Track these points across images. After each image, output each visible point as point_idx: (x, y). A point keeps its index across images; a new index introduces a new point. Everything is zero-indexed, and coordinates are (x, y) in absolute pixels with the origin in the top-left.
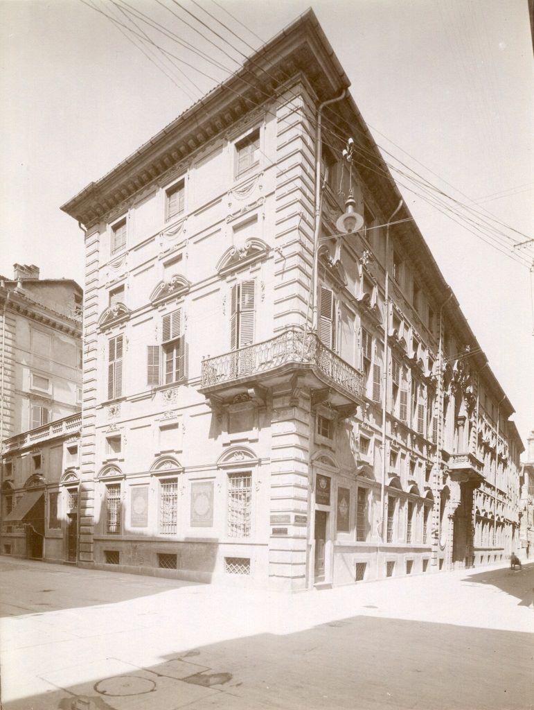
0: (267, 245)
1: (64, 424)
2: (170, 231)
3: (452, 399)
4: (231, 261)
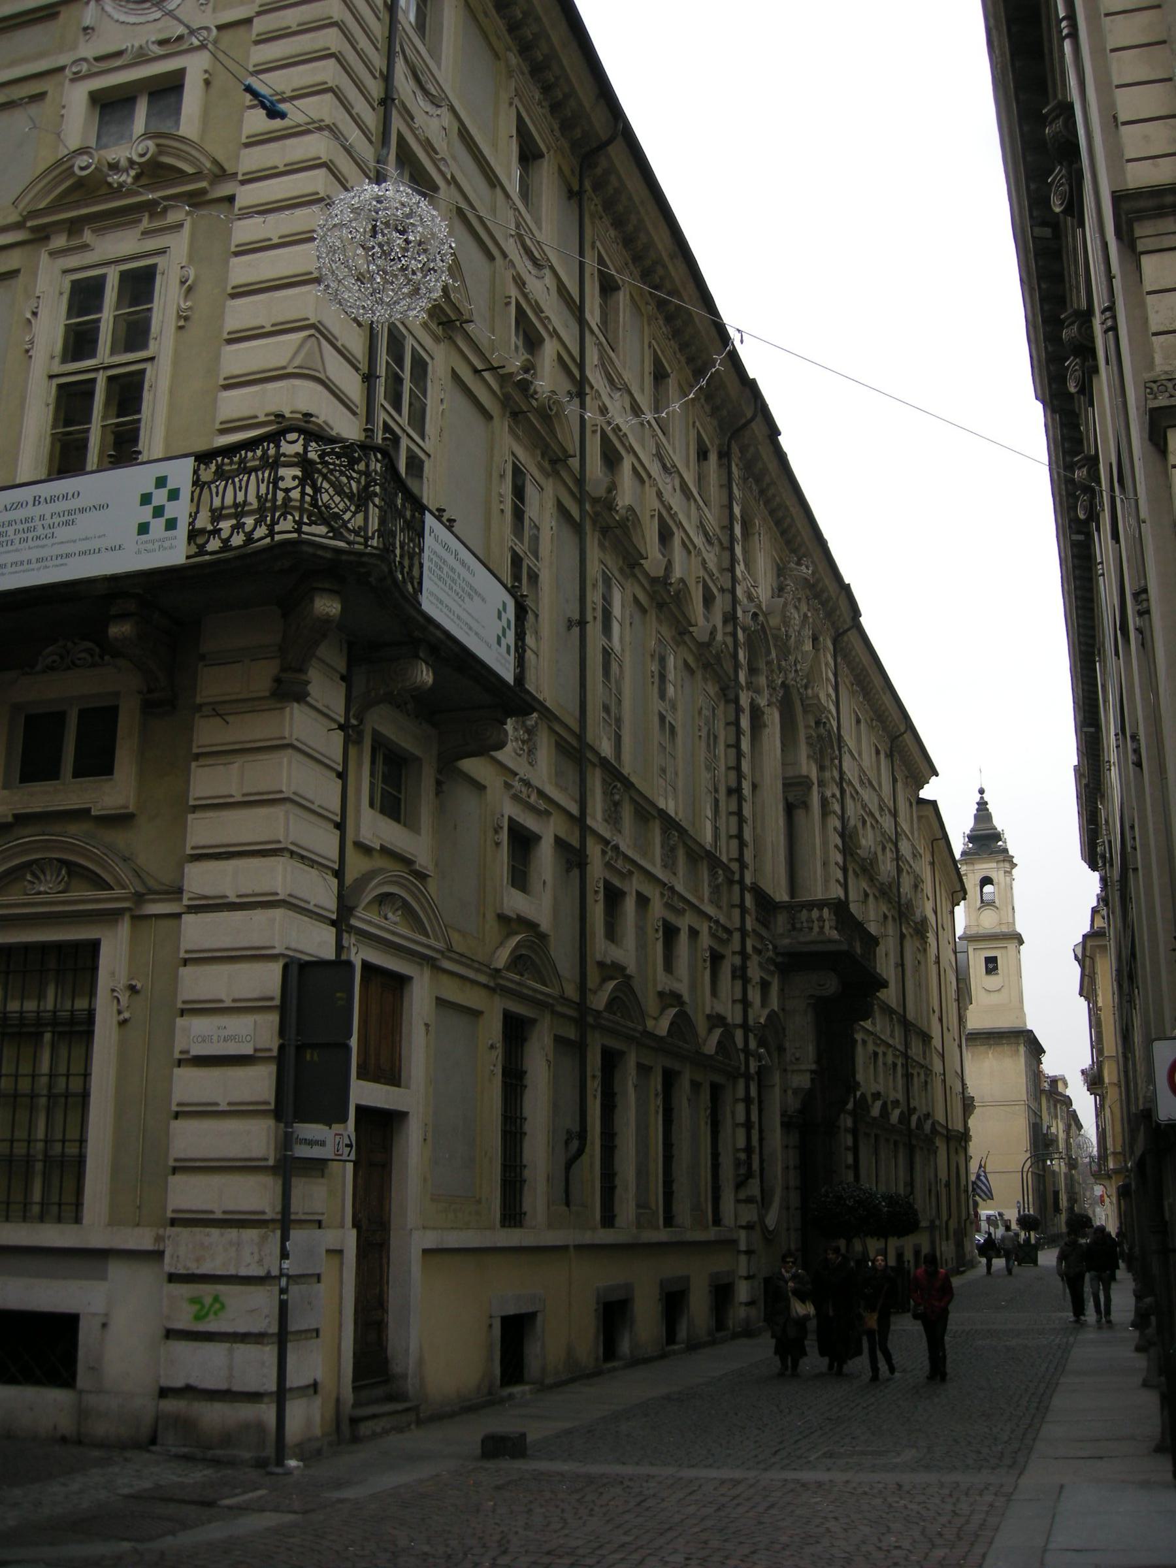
0: (215, 162)
3: (773, 718)
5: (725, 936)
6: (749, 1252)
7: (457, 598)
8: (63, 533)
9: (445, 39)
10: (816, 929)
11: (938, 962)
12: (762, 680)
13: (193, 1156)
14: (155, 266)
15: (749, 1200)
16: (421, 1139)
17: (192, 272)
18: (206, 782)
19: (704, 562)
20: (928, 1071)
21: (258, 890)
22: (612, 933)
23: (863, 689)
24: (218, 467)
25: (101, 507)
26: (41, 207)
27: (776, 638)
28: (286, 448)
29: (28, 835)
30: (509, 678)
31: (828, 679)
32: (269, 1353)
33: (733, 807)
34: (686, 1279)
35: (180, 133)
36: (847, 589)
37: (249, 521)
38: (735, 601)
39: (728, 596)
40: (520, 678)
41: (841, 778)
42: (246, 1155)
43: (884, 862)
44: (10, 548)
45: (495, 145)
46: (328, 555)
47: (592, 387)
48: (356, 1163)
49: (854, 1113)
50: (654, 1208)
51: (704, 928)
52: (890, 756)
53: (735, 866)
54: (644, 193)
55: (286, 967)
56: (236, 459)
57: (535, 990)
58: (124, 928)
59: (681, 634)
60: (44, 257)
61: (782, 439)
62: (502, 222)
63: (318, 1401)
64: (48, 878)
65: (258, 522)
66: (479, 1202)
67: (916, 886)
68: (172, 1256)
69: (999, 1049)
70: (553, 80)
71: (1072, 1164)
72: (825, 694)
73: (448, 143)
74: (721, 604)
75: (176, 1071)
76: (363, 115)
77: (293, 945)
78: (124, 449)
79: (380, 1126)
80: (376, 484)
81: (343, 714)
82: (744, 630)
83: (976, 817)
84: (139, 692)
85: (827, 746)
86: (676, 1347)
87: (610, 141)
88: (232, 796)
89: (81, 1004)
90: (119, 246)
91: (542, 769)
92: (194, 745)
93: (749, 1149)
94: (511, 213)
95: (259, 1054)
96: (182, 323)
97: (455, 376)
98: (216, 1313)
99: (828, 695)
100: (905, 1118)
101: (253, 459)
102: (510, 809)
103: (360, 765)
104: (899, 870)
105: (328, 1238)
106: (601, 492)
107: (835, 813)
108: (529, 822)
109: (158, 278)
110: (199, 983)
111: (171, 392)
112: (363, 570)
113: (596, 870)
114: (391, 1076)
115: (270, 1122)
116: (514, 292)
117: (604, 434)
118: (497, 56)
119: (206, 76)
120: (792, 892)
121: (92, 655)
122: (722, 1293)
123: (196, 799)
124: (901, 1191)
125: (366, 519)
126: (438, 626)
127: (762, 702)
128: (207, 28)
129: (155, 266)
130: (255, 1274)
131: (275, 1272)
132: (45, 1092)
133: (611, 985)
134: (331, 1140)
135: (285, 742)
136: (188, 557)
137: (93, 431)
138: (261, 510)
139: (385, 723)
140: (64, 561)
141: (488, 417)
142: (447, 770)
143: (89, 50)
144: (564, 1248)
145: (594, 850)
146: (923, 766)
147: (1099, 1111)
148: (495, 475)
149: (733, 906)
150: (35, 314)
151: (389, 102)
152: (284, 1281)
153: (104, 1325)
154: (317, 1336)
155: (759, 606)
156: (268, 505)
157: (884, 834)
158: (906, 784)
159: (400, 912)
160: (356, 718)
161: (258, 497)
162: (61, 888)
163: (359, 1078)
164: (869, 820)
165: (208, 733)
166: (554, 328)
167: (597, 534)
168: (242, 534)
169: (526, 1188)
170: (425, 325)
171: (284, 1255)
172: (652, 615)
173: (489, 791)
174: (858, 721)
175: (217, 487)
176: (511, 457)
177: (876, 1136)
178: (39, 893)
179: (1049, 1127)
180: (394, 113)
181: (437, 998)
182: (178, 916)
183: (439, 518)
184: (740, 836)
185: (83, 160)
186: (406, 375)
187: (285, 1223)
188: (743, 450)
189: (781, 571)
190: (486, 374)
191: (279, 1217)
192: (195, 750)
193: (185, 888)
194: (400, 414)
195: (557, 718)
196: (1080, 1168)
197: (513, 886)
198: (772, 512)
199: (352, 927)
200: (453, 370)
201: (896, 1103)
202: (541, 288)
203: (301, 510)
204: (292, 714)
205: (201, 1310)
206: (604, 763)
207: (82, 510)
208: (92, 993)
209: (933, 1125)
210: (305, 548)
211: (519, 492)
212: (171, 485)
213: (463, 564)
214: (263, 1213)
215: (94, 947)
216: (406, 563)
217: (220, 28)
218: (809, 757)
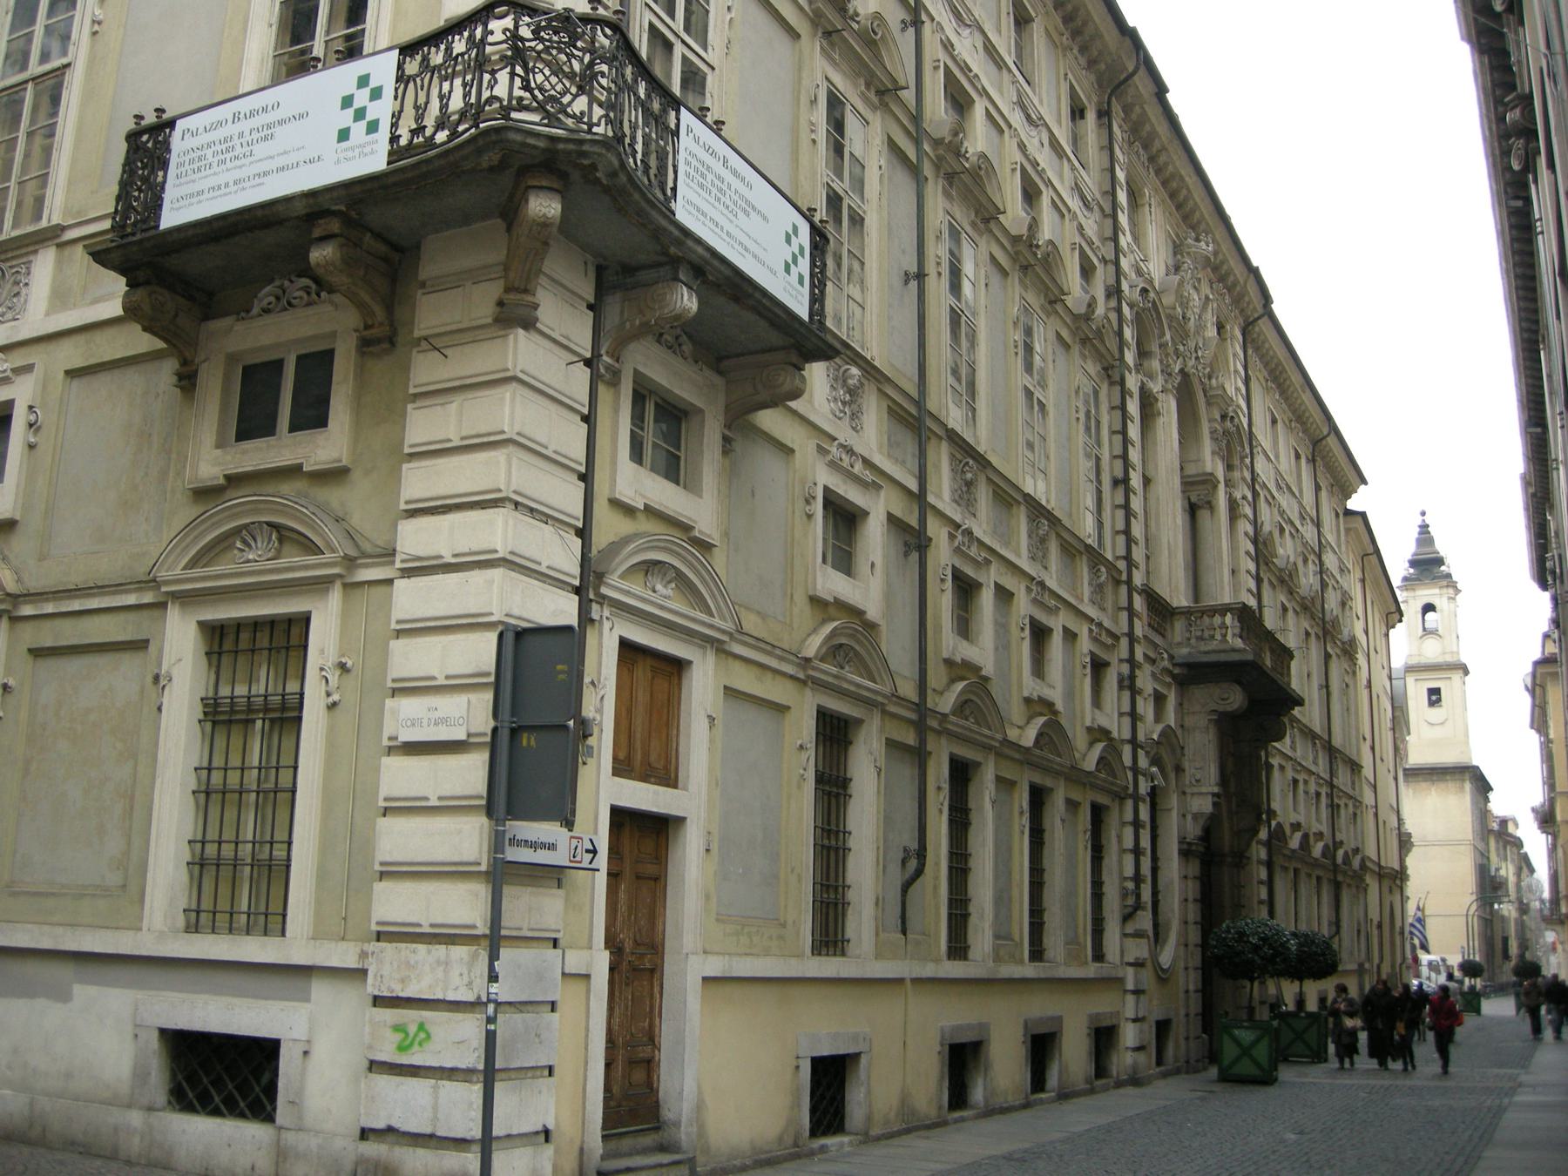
3: (1168, 407)
5: (1109, 641)
6: (1137, 992)
8: (260, 150)
10: (1218, 637)
11: (1369, 686)
12: (1155, 365)
13: (400, 859)
15: (1139, 934)
16: (702, 849)
18: (423, 426)
19: (1080, 228)
20: (1358, 803)
21: (475, 548)
22: (964, 627)
23: (1279, 386)
25: (301, 116)
27: (1170, 318)
30: (803, 312)
31: (1236, 371)
33: (1120, 500)
34: (1059, 1019)
36: (1255, 272)
38: (1118, 272)
39: (1111, 268)
41: (1253, 479)
42: (456, 859)
43: (1305, 575)
44: (208, 172)
46: (541, 144)
49: (1268, 844)
50: (1017, 938)
51: (1083, 631)
52: (1312, 461)
53: (1122, 565)
54: (1203, 192)
57: (858, 686)
58: (335, 596)
59: (1051, 302)
61: (1171, 98)
63: (549, 1150)
66: (784, 925)
67: (1343, 604)
69: (1442, 785)
71: (1523, 909)
72: (1233, 386)
74: (1102, 276)
75: (386, 760)
79: (643, 838)
81: (590, 347)
82: (1131, 306)
83: (1418, 541)
85: (1236, 444)
86: (1043, 1096)
88: (449, 440)
91: (871, 435)
93: (1137, 878)
95: (472, 740)
98: (420, 1044)
99: (1237, 389)
100: (1329, 852)
102: (825, 477)
104: (1324, 585)
106: (944, 132)
107: (1245, 516)
112: (586, 162)
113: (942, 554)
114: (666, 774)
115: (483, 820)
117: (948, 73)
120: (1196, 598)
121: (308, 293)
122: (1103, 1038)
124: (1325, 931)
126: (699, 241)
127: (1155, 387)
130: (464, 999)
133: (960, 686)
135: (509, 374)
140: (261, 180)
141: (794, 35)
144: (899, 981)
145: (935, 529)
146: (1352, 475)
147: (1552, 851)
148: (804, 100)
149: (1120, 609)
152: (491, 1008)
155: (1151, 282)
157: (1305, 544)
158: (1331, 493)
160: (610, 354)
162: (270, 555)
164: (1287, 528)
167: (941, 182)
169: (850, 912)
171: (493, 977)
172: (1015, 277)
173: (797, 454)
174: (1274, 421)
176: (826, 83)
177: (1296, 871)
178: (249, 561)
179: (1497, 870)
183: (702, 119)
184: (1127, 532)
187: (495, 940)
188: (1127, 109)
189: (1177, 248)
191: (488, 932)
192: (412, 391)
194: (673, 17)
195: (888, 380)
196: (1532, 913)
198: (1164, 183)
199: (604, 597)
200: (889, 137)
201: (1320, 835)
204: (516, 341)
206: (953, 437)
207: (281, 122)
209: (1363, 860)
210: (512, 136)
212: (373, 83)
213: (735, 173)
214: (474, 927)
215: (306, 619)
216: (653, 163)
218: (1213, 453)
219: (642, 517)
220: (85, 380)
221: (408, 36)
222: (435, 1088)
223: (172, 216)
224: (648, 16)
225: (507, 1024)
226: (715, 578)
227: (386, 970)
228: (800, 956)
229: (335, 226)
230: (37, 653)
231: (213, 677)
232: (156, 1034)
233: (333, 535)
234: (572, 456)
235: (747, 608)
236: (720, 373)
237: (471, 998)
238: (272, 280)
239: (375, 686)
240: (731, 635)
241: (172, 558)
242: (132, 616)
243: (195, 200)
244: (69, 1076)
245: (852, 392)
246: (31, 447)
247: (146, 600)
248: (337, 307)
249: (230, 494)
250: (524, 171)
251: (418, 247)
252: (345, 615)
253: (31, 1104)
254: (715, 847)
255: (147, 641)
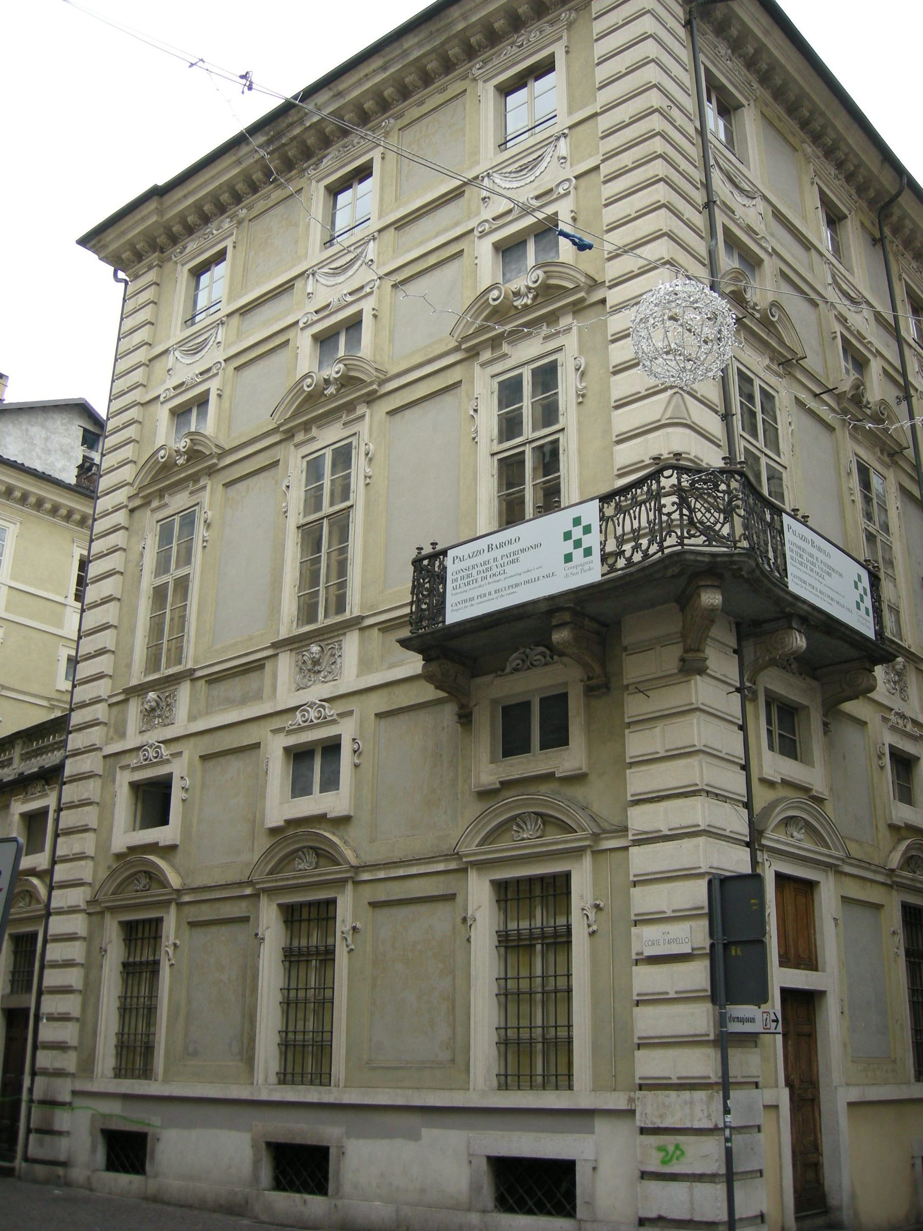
0: (588, 276)
1: (285, 663)
2: (334, 265)
4: (305, 401)
7: (817, 577)
8: (511, 569)
9: (750, 145)
14: (556, 360)
17: (583, 361)
18: (637, 744)
21: (684, 824)
24: (617, 504)
25: (536, 546)
26: (471, 332)
28: (664, 482)
29: (511, 797)
30: (871, 634)
32: (720, 1189)
35: (560, 260)
37: (644, 542)
40: (880, 633)
42: (692, 1032)
44: (475, 585)
45: (804, 218)
46: (707, 559)
47: (916, 390)
48: (785, 1035)
55: (710, 882)
56: (629, 496)
58: (587, 860)
60: (477, 368)
62: (820, 277)
64: (529, 827)
65: (651, 542)
66: (894, 1061)
68: (641, 1114)
70: (843, 157)
73: (766, 225)
76: (692, 219)
77: (715, 865)
78: (550, 500)
79: (802, 1005)
80: (738, 499)
84: (582, 681)
87: (899, 194)
89: (561, 921)
90: (526, 352)
92: (626, 716)
94: (826, 267)
96: (580, 400)
97: (799, 402)
98: (677, 1159)
101: (642, 494)
102: (890, 738)
103: (757, 718)
105: (767, 1096)
108: (909, 747)
109: (559, 368)
110: (646, 900)
111: (579, 452)
112: (735, 567)
114: (810, 962)
115: (709, 1005)
116: (838, 328)
118: (795, 150)
119: (573, 214)
121: (545, 657)
123: (631, 758)
125: (732, 527)
126: (804, 602)
128: (568, 180)
129: (556, 360)
131: (721, 1125)
132: (540, 990)
134: (760, 1016)
135: (694, 706)
136: (602, 575)
137: (527, 490)
138: (652, 532)
139: (776, 682)
141: (830, 428)
142: (831, 710)
143: (488, 213)
148: (843, 474)
150: (476, 411)
151: (711, 204)
152: (727, 1132)
153: (594, 1169)
154: (761, 1176)
156: (657, 527)
159: (803, 831)
160: (749, 680)
161: (649, 522)
163: (782, 964)
165: (635, 707)
166: (877, 350)
168: (640, 552)
170: (768, 367)
171: (727, 1111)
173: (870, 726)
175: (618, 519)
176: (855, 458)
180: (717, 211)
181: (842, 897)
182: (626, 848)
183: (794, 517)
185: (495, 293)
186: (758, 409)
187: (725, 1085)
190: (824, 396)
191: (720, 1081)
192: (627, 720)
193: (629, 826)
197: (900, 800)
199: (763, 846)
200: (900, 485)
202: (861, 321)
203: (681, 526)
204: (696, 684)
205: (665, 1157)
207: (523, 550)
208: (568, 912)
210: (688, 557)
211: (866, 484)
212: (584, 523)
213: (819, 549)
214: (709, 1077)
215: (567, 876)
217: (576, 178)
219: (779, 787)
220: (390, 719)
221: (605, 489)
222: (691, 1188)
223: (453, 615)
224: (743, 443)
225: (738, 1140)
226: (830, 823)
227: (649, 1110)
228: (908, 1083)
229: (567, 617)
230: (374, 905)
231: (502, 916)
232: (485, 1160)
233: (585, 821)
234: (736, 754)
235: (851, 840)
236: (815, 678)
237: (710, 1125)
238: (517, 649)
239: (621, 920)
240: (843, 860)
241: (468, 839)
242: (441, 878)
243: (468, 604)
244: (423, 1191)
245: (898, 674)
246: (356, 766)
247: (451, 867)
248: (565, 665)
249: (505, 794)
250: (697, 575)
251: (619, 623)
252: (596, 871)
253: (397, 1211)
254: (846, 1010)
255: (455, 894)
